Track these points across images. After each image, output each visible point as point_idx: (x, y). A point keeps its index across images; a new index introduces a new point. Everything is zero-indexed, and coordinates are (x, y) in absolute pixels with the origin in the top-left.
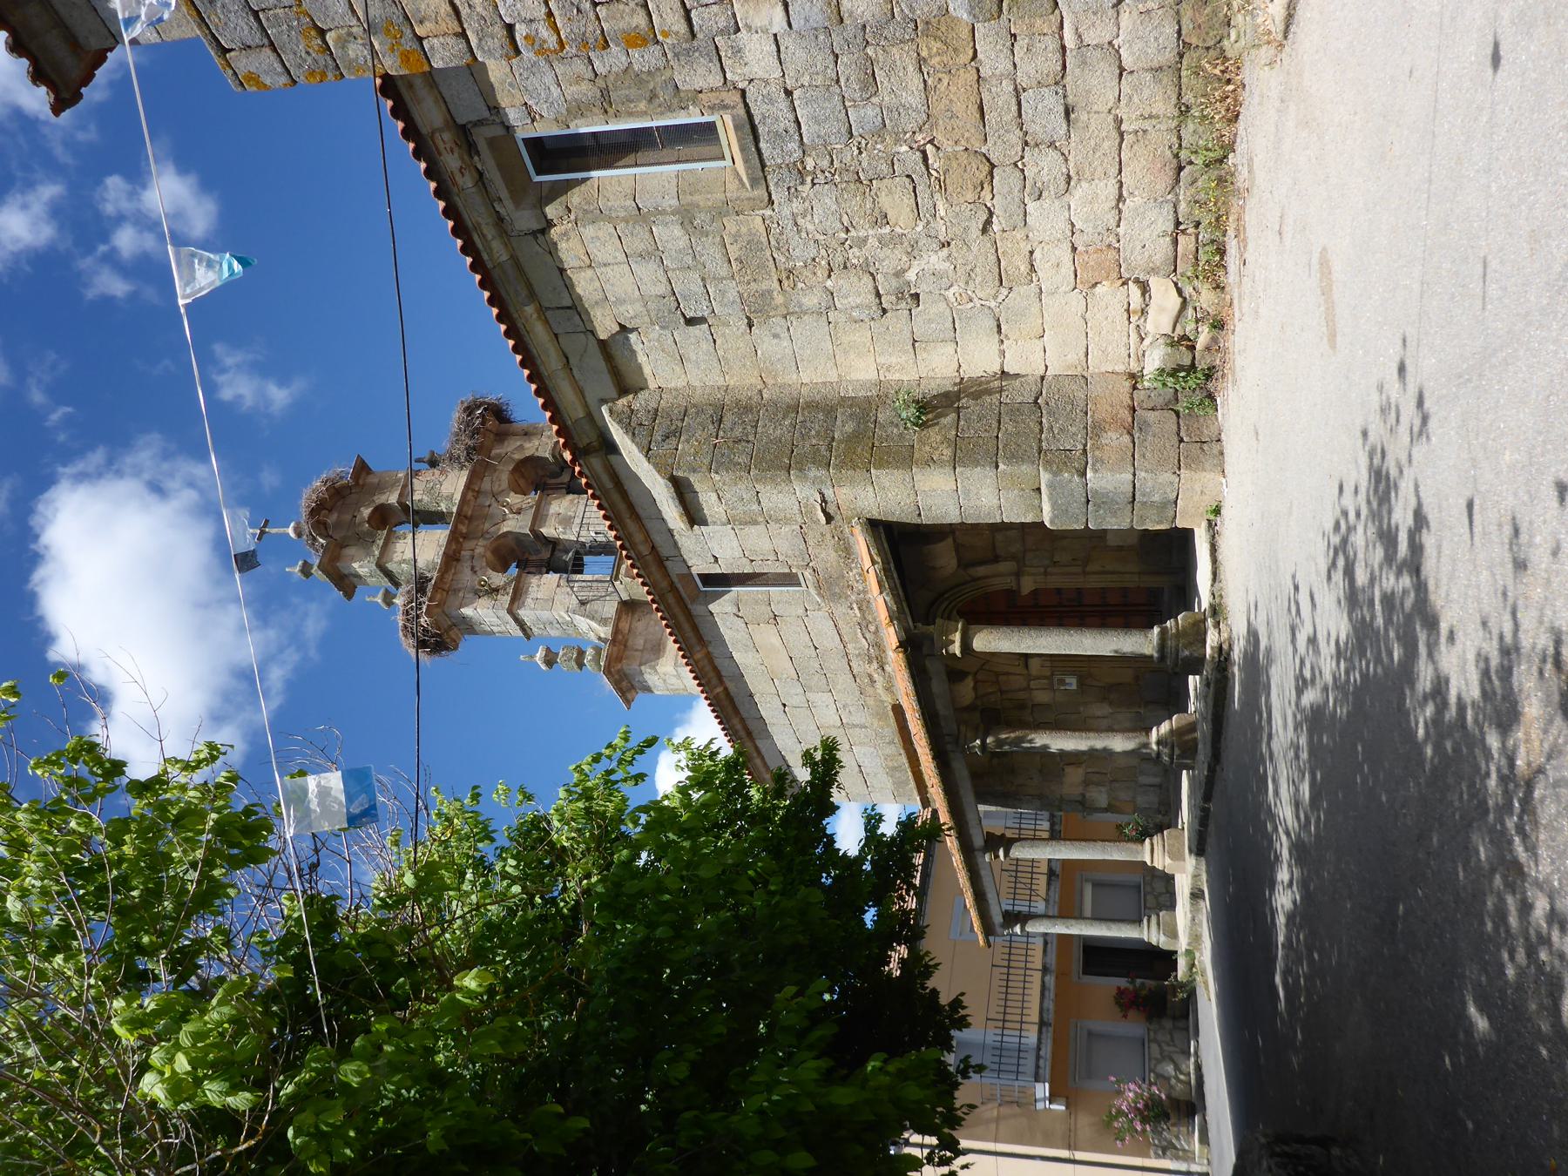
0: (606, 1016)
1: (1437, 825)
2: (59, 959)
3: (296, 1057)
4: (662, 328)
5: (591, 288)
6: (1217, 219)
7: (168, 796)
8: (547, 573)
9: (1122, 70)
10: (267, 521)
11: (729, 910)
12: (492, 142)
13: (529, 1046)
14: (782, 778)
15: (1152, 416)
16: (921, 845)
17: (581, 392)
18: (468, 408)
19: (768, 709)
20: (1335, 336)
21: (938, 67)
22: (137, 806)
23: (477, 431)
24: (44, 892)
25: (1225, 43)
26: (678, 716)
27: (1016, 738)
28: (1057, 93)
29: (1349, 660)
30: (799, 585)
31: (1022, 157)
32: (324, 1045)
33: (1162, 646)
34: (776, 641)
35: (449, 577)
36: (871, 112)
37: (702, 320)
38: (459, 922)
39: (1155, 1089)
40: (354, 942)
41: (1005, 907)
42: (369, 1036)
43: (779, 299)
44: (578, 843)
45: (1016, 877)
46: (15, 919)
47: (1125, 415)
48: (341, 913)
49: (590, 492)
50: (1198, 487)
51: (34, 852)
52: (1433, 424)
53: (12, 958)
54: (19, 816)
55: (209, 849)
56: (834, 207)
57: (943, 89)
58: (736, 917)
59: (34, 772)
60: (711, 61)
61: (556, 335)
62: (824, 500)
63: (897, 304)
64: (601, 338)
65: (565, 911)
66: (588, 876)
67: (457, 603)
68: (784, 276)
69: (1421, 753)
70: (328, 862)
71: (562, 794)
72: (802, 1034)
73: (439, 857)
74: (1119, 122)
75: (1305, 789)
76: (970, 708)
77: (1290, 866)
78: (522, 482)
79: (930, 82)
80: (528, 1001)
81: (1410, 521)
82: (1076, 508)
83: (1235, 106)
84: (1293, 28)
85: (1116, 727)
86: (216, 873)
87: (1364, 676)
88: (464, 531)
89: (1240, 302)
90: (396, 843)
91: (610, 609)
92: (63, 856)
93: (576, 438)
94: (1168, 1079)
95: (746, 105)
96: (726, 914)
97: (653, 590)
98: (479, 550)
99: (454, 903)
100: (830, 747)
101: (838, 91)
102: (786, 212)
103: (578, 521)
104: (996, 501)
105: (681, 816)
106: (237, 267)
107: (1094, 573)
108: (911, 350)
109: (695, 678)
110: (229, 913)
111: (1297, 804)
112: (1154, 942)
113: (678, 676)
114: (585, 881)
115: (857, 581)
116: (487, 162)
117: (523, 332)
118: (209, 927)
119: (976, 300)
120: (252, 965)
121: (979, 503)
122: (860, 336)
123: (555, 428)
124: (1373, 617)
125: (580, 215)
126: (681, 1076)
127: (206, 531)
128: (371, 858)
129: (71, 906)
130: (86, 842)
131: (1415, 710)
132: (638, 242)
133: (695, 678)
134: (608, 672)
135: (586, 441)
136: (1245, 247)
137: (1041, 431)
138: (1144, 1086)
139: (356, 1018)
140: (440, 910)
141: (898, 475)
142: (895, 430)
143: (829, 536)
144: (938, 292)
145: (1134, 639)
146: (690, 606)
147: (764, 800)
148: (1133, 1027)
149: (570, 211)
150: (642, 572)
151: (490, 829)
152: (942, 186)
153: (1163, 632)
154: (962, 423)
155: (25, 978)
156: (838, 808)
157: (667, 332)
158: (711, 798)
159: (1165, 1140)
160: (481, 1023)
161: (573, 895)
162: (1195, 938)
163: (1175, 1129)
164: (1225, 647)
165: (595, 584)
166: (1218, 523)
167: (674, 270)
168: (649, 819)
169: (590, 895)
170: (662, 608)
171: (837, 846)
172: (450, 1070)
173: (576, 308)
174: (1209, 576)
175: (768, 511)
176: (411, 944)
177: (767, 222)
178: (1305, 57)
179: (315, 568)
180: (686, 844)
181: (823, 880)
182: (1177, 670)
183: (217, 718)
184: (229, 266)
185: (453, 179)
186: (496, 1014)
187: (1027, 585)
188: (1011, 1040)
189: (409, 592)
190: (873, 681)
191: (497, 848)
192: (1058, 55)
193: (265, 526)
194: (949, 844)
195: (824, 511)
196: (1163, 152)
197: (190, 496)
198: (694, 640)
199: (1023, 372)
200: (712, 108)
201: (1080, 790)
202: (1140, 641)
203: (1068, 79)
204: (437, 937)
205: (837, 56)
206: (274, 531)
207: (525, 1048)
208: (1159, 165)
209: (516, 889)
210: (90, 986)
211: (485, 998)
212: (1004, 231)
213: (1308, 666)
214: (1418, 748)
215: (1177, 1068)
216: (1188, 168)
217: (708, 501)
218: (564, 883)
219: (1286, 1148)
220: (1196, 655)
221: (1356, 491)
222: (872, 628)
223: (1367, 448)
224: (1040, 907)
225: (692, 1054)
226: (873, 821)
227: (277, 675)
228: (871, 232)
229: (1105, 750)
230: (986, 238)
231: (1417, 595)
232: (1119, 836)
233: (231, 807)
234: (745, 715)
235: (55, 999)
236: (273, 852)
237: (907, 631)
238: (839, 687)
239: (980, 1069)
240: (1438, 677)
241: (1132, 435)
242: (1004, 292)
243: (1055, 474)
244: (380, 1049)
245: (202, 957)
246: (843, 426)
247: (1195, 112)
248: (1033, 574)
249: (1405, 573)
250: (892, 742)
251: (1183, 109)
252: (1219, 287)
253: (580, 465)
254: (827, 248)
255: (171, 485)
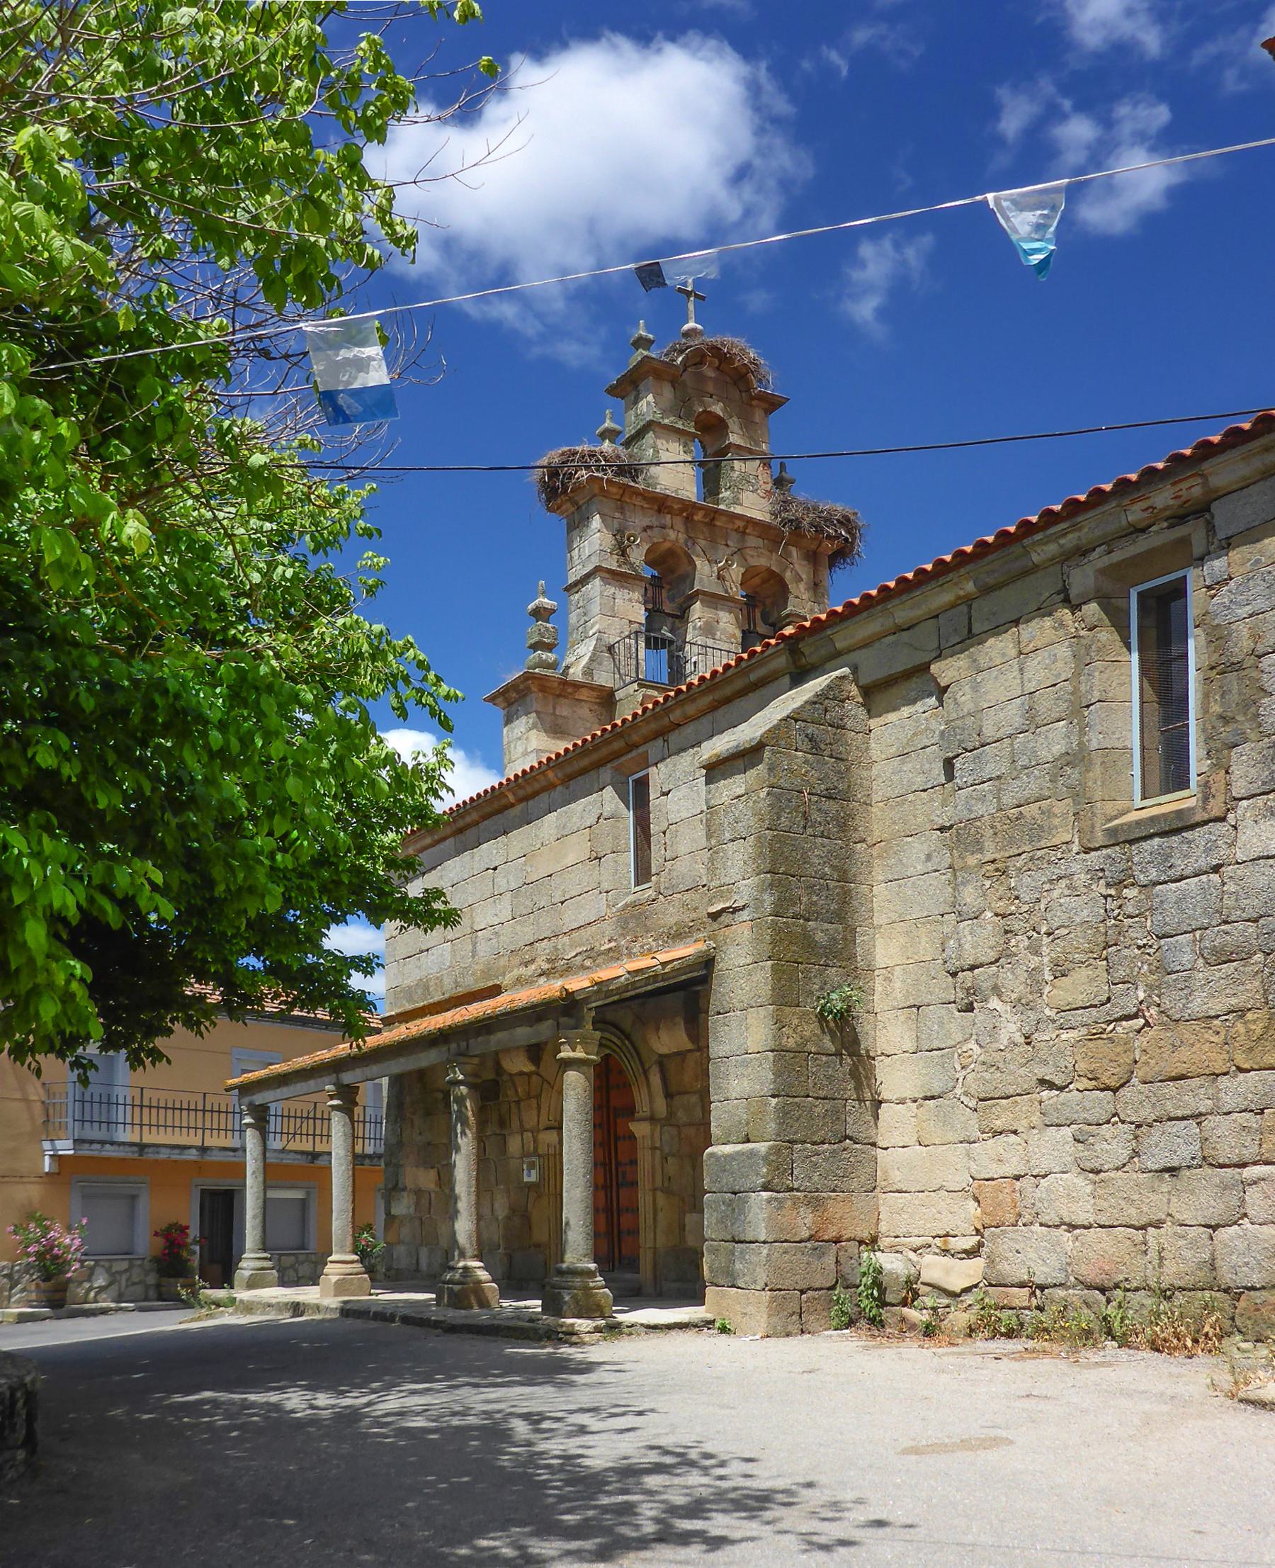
0: (106, 677)
1: (382, 1559)
2: (117, 66)
3: (12, 333)
4: (942, 733)
5: (993, 654)
6: (1045, 1330)
7: (345, 191)
8: (646, 610)
9: (1215, 1228)
10: (703, 298)
11: (249, 811)
12: (1185, 542)
13: (58, 592)
14: (411, 867)
15: (830, 1260)
16: (339, 1016)
17: (866, 645)
18: (848, 520)
19: (490, 851)
20: (917, 1454)
21: (1233, 1030)
22: (328, 157)
23: (819, 530)
24: (204, 51)
25: (1238, 1337)
26: (479, 753)
27: (467, 1118)
28: (1193, 1158)
29: (561, 1469)
30: (637, 884)
31: (1123, 1122)
32: (33, 364)
33: (573, 1272)
34: (570, 860)
35: (638, 501)
36: (1186, 958)
37: (950, 776)
38: (209, 515)
39: (76, 1266)
40: (171, 398)
41: (272, 1106)
42: (51, 416)
43: (972, 860)
44: (318, 646)
45: (308, 1118)
46: (166, 16)
47: (832, 1233)
48: (209, 384)
49: (745, 656)
50: (750, 1309)
51: (257, 39)
52: (821, 1556)
53: (113, 13)
54: (304, 22)
55: (277, 237)
56: (1078, 920)
57: (1206, 1036)
58: (241, 818)
59: (363, 38)
60: (1264, 783)
61: (937, 616)
62: (736, 910)
63: (962, 988)
64: (932, 667)
65: (233, 632)
66: (278, 656)
67: (606, 511)
68: (1000, 866)
69: (461, 1543)
70: (273, 371)
71: (377, 628)
72: (106, 890)
73: (289, 493)
74: (1157, 1225)
75: (419, 1423)
76: (499, 1069)
77: (333, 1406)
78: (757, 580)
79: (1216, 1022)
80: (114, 591)
81: (715, 1532)
82: (726, 1180)
83: (1168, 1348)
84: (1250, 1408)
85: (482, 1223)
86: (248, 245)
87: (544, 1485)
88: (696, 518)
89: (954, 1353)
90: (303, 445)
91: (604, 678)
92: (254, 72)
93: (810, 640)
94: (89, 1279)
95: (1205, 823)
96: (243, 806)
97: (628, 724)
98: (672, 535)
99: (233, 510)
100: (450, 918)
101: (1214, 923)
102: (1075, 867)
103: (710, 642)
104: (734, 1095)
105: (358, 758)
106: (1036, 258)
107: (654, 1200)
108: (908, 1004)
109: (524, 772)
110: (196, 259)
111: (401, 1414)
112: (243, 1264)
113: (526, 754)
114: (271, 653)
115: (642, 947)
116: (1159, 537)
117: (941, 581)
118: (176, 236)
119: (964, 1073)
120: (130, 284)
121: (732, 1077)
122: (926, 948)
123: (823, 617)
124: (609, 1494)
125: (1084, 642)
126: (38, 759)
127: (688, 229)
128: (282, 418)
129: (188, 80)
130: (278, 99)
131: (508, 1537)
132: (1046, 704)
133: (524, 772)
134: (527, 677)
135: (806, 651)
136: (1015, 1359)
137: (814, 1143)
138: (79, 1255)
139: (72, 400)
140: (222, 493)
141: (766, 991)
142: (816, 987)
143: (694, 915)
144: (974, 1032)
145: (582, 1243)
146: (609, 765)
147: (382, 847)
148: (146, 1243)
149: (1090, 630)
150: (648, 713)
151: (328, 549)
152: (1094, 1037)
153: (590, 1274)
154: (824, 1058)
155: (86, 26)
156: (378, 928)
157: (936, 739)
158: (381, 790)
159: (20, 1277)
160: (81, 540)
161: (253, 640)
162: (248, 1308)
163: (33, 1287)
164: (574, 1339)
165: (634, 662)
166: (711, 1332)
167: (1012, 745)
168: (353, 722)
169: (255, 658)
170: (607, 736)
171: (333, 926)
172: (16, 505)
173: (969, 638)
174: (653, 1321)
175: (724, 851)
176: (176, 462)
177: (1064, 847)
178: (1218, 1421)
179: (646, 353)
180: (325, 764)
181: (292, 912)
182: (548, 1288)
183: (448, 245)
184: (1037, 250)
185: (1140, 499)
186: (95, 556)
187: (640, 1129)
188: (119, 1114)
189: (618, 457)
190: (526, 964)
191: (305, 556)
192: (1236, 1160)
193: (696, 296)
194: (342, 1046)
195: (723, 910)
196: (1122, 1272)
197: (733, 211)
198: (569, 770)
199: (880, 1123)
200: (1206, 785)
201: (410, 1185)
202: (580, 1248)
203: (1209, 1170)
204: (187, 490)
205: (1256, 921)
206: (691, 306)
207: (55, 589)
208: (1107, 1268)
209: (256, 578)
210: (83, 101)
211: (115, 544)
212: (1040, 1103)
213: (555, 1426)
214: (466, 1540)
215: (102, 1289)
216: (1103, 1299)
217: (735, 785)
218: (268, 630)
219: (20, 1404)
220: (565, 1308)
221: (746, 1476)
222: (588, 963)
223: (794, 1487)
224: (276, 1143)
225: (69, 771)
226: (366, 964)
227: (507, 311)
228: (1046, 960)
229: (457, 1212)
230: (1034, 1083)
231: (634, 1539)
232: (359, 1227)
233: (335, 261)
234: (482, 826)
235: (60, 61)
236: (280, 308)
237: (586, 1000)
238: (519, 927)
239: (84, 1081)
240: (544, 1561)
241: (808, 1240)
242: (972, 1104)
243: (765, 1158)
244: (35, 427)
245: (135, 228)
246: (822, 931)
247: (1164, 1306)
248: (652, 1135)
249: (658, 1527)
250: (457, 984)
251: (1168, 1293)
252: (971, 1331)
253: (777, 644)
254: (1030, 912)
255: (747, 191)
